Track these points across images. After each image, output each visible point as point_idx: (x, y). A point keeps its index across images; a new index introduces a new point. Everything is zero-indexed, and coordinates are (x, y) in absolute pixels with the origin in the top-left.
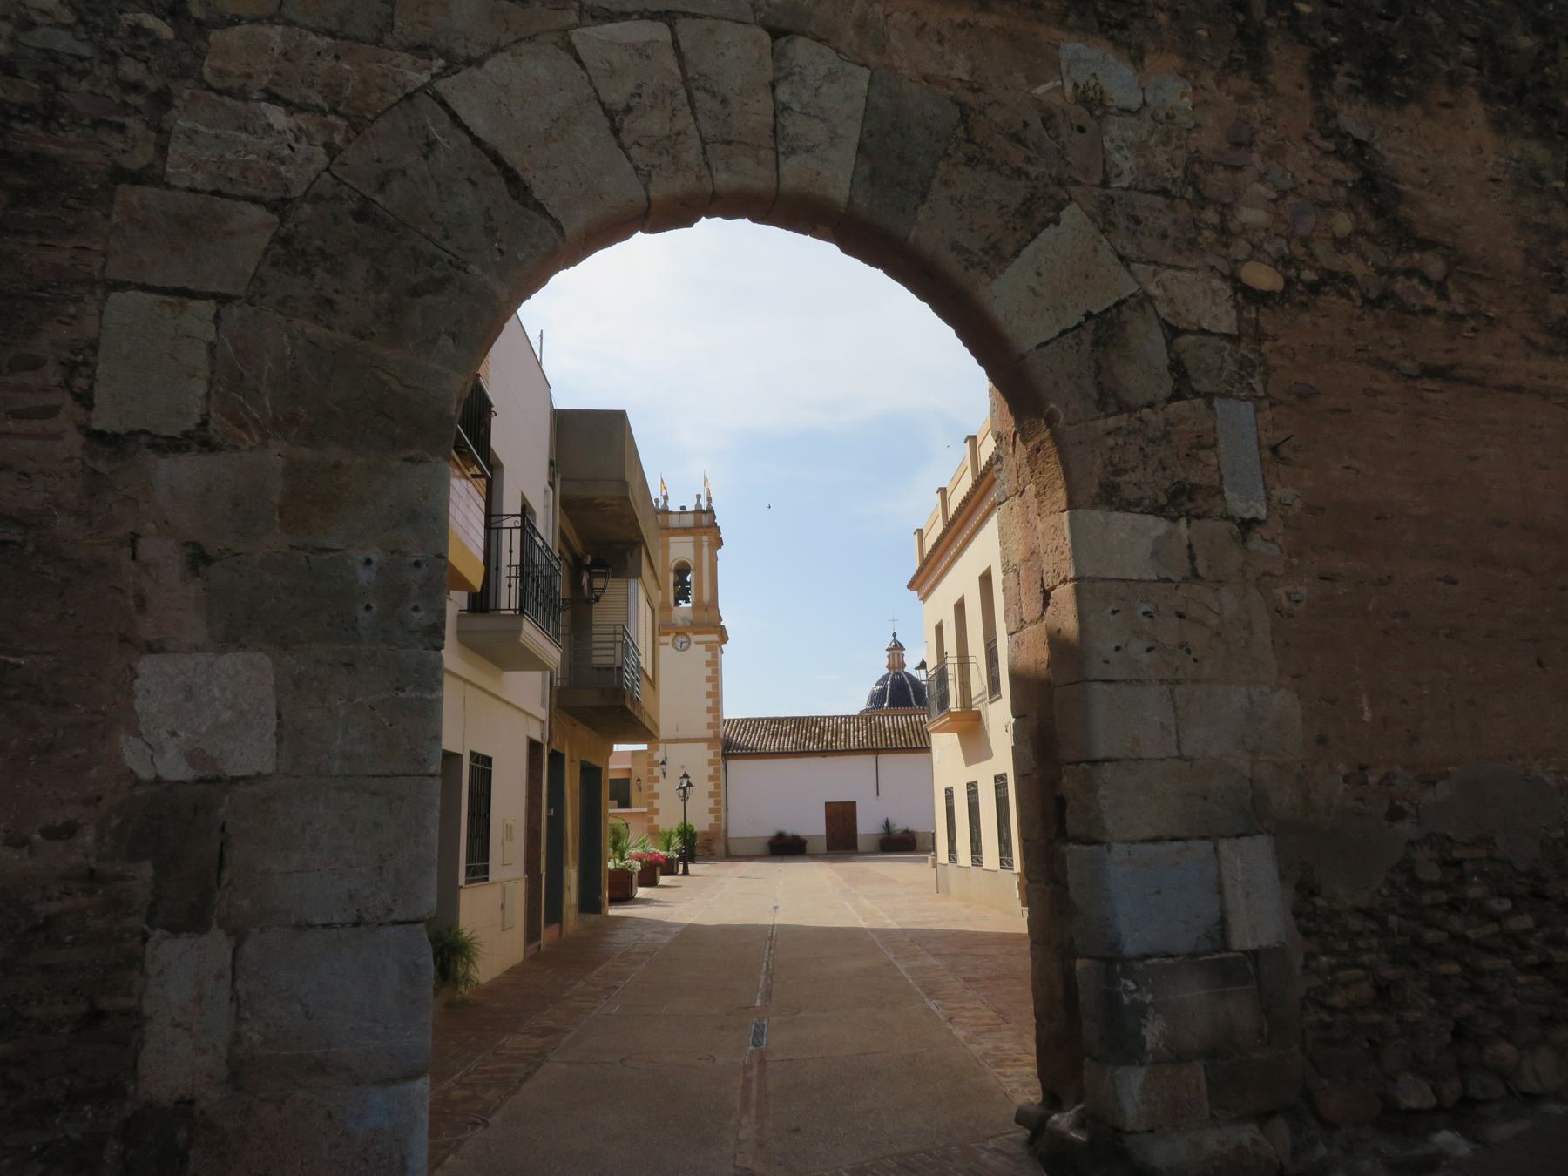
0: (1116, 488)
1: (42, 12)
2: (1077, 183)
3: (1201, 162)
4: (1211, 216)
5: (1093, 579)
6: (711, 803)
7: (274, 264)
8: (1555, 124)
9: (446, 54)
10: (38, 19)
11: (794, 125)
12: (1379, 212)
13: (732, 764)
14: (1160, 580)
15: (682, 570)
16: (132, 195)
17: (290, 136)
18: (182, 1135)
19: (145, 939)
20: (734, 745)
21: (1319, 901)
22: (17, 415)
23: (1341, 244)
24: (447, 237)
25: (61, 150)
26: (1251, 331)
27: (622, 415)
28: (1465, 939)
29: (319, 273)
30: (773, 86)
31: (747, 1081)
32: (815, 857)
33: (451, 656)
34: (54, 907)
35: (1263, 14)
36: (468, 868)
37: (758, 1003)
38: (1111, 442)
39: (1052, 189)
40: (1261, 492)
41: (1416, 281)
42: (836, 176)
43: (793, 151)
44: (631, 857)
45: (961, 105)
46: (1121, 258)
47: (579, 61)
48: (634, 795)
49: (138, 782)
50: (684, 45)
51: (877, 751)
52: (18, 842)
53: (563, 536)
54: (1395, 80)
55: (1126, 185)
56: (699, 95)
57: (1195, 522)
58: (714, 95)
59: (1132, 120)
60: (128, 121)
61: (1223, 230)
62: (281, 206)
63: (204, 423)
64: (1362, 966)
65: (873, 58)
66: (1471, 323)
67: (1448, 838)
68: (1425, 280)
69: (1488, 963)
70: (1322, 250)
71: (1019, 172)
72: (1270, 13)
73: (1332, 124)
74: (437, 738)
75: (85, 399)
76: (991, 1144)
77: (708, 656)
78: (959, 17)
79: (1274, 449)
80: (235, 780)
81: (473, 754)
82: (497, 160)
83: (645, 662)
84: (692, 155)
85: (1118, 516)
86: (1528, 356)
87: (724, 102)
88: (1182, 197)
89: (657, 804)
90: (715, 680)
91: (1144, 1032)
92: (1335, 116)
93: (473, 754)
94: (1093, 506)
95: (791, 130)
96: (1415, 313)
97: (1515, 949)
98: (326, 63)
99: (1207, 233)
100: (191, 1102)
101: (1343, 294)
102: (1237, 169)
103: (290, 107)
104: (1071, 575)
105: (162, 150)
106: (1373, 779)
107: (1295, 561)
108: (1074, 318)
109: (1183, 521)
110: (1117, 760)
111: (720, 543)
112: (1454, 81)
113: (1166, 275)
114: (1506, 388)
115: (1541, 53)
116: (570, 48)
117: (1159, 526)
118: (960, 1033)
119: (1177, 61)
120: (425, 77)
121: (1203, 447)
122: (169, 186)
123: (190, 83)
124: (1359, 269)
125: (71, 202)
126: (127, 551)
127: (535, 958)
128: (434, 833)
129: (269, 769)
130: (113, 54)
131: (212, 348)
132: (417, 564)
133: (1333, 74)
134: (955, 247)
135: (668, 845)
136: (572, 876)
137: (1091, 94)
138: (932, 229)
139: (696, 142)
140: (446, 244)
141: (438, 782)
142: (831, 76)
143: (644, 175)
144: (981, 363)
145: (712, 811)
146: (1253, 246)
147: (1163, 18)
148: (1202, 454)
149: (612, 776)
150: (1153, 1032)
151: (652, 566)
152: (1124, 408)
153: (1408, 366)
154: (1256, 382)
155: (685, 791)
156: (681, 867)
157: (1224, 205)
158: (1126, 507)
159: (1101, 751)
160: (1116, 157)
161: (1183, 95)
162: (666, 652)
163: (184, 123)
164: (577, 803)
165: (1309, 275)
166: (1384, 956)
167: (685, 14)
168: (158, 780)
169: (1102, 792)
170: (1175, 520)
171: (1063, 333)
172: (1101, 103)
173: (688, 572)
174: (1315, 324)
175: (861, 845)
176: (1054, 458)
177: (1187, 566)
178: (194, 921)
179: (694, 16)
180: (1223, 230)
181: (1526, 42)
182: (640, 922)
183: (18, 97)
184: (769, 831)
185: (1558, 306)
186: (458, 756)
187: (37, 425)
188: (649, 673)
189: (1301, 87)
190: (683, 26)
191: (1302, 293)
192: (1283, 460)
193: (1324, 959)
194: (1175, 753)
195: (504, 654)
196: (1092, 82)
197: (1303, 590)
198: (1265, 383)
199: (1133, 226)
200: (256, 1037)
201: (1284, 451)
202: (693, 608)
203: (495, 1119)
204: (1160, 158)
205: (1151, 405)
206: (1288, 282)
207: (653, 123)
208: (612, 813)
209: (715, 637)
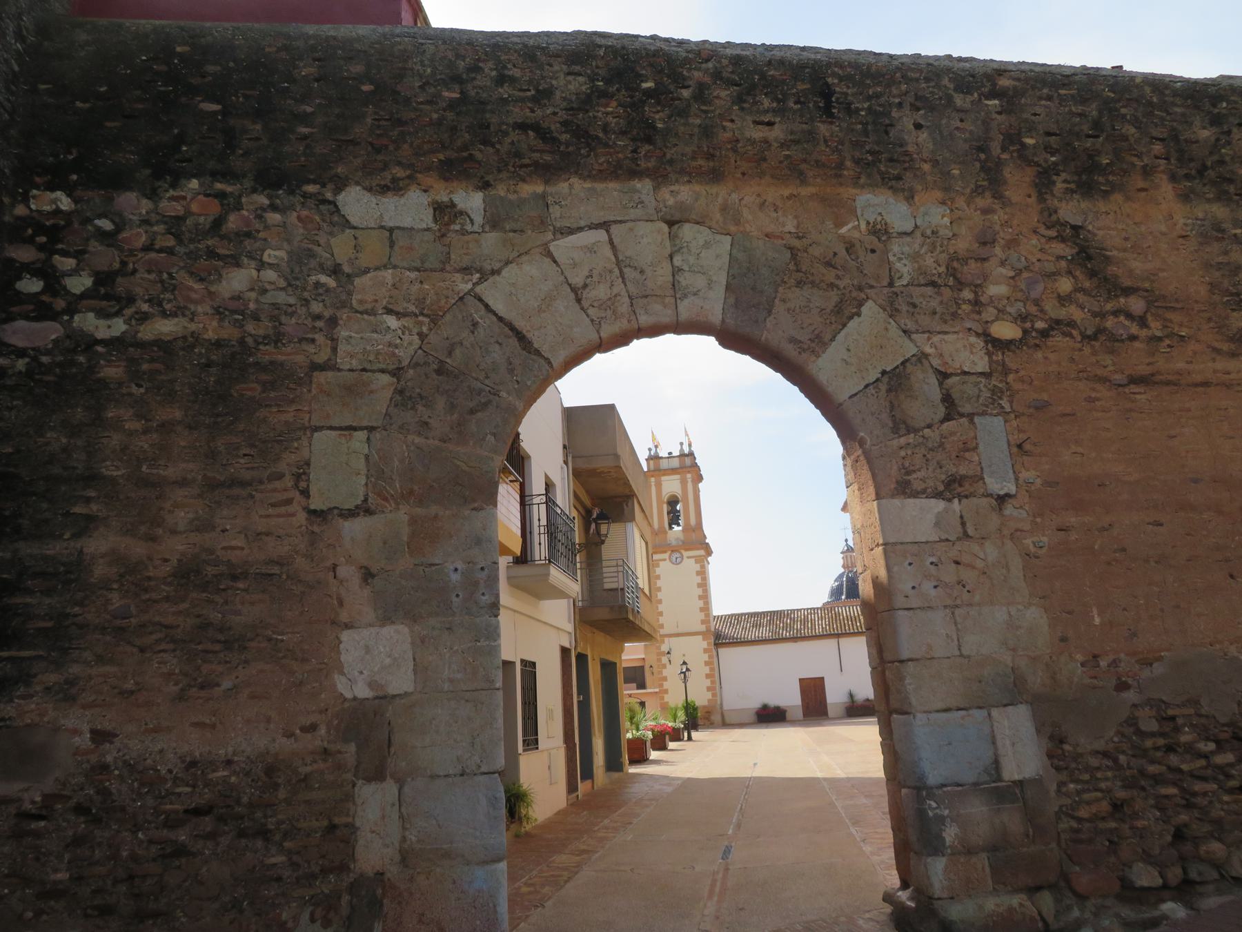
0: (908, 483)
1: (270, 283)
2: (872, 287)
3: (958, 260)
4: (967, 294)
5: (895, 544)
6: (708, 683)
7: (396, 406)
8: (1232, 189)
9: (480, 271)
10: (268, 287)
11: (685, 280)
12: (1092, 274)
13: (722, 651)
14: (941, 541)
15: (673, 502)
16: (321, 377)
17: (400, 332)
18: (379, 891)
19: (354, 786)
20: (723, 637)
21: (1067, 747)
22: (273, 505)
23: (1063, 300)
24: (487, 377)
25: (284, 358)
26: (1000, 368)
27: (611, 408)
28: (1180, 771)
29: (420, 408)
30: (671, 257)
31: (714, 881)
32: (794, 723)
33: (506, 597)
34: (309, 769)
35: (999, 151)
36: (524, 741)
37: (730, 832)
38: (903, 453)
39: (854, 294)
40: (1011, 475)
41: (1122, 318)
42: (715, 305)
43: (685, 296)
44: (646, 729)
45: (791, 249)
46: (905, 332)
47: (555, 262)
48: (649, 679)
49: (345, 699)
50: (616, 241)
51: (838, 636)
52: (289, 735)
53: (576, 496)
54: (1101, 179)
55: (905, 283)
56: (626, 270)
57: (964, 501)
58: (635, 268)
59: (908, 239)
60: (316, 336)
61: (976, 303)
62: (396, 373)
63: (366, 500)
64: (1101, 790)
65: (733, 229)
66: (1167, 342)
67: (1163, 702)
68: (1129, 316)
69: (1198, 787)
70: (1048, 307)
71: (832, 286)
72: (1004, 149)
73: (1054, 218)
74: (495, 650)
75: (306, 493)
76: (867, 915)
77: (698, 567)
78: (787, 192)
79: (1020, 446)
80: (394, 696)
81: (522, 661)
82: (512, 328)
83: (643, 582)
84: (624, 308)
85: (911, 501)
86: (1214, 360)
87: (642, 272)
88: (946, 285)
89: (666, 685)
90: (704, 585)
91: (944, 835)
92: (1056, 212)
93: (522, 661)
94: (893, 496)
95: (684, 283)
96: (1122, 341)
97: (1221, 777)
98: (417, 286)
99: (964, 307)
100: (382, 874)
101: (1065, 334)
102: (985, 260)
103: (399, 315)
104: (881, 541)
105: (334, 350)
106: (1103, 664)
107: (1039, 520)
108: (874, 375)
109: (956, 501)
110: (917, 660)
111: (700, 478)
112: (1147, 172)
113: (936, 339)
114: (1196, 385)
115: (1218, 140)
116: (549, 255)
117: (940, 505)
118: (867, 849)
119: (939, 194)
120: (470, 286)
121: (968, 450)
122: (339, 370)
123: (346, 310)
124: (1077, 314)
125: (291, 386)
126: (331, 574)
127: (576, 805)
128: (500, 722)
129: (411, 689)
130: (306, 300)
131: (367, 457)
132: (482, 569)
133: (1054, 183)
134: (793, 340)
135: (675, 718)
136: (598, 744)
137: (879, 227)
138: (775, 332)
139: (627, 300)
140: (487, 382)
141: (500, 693)
142: (707, 245)
143: (596, 324)
144: (817, 407)
145: (709, 689)
146: (999, 311)
147: (926, 167)
148: (967, 455)
149: (624, 665)
150: (950, 834)
151: (643, 511)
152: (910, 430)
153: (1118, 378)
154: (1005, 403)
155: (684, 675)
156: (686, 734)
157: (976, 286)
158: (915, 495)
159: (905, 655)
160: (898, 265)
161: (943, 216)
162: (665, 568)
163: (344, 333)
164: (598, 686)
165: (1040, 325)
166: (1119, 783)
167: (615, 222)
168: (355, 699)
169: (907, 681)
170: (950, 500)
171: (867, 386)
172: (886, 232)
173: (677, 502)
174: (1046, 358)
175: (831, 713)
176: (866, 467)
177: (960, 529)
178: (378, 775)
179: (621, 222)
180: (976, 303)
181: (1205, 134)
182: (651, 776)
183: (261, 332)
184: (756, 704)
185: (1241, 320)
186: (513, 663)
187: (282, 510)
188: (647, 591)
189: (1030, 196)
190: (615, 229)
191: (1035, 338)
192: (1026, 453)
193: (1072, 786)
194: (957, 653)
195: (541, 590)
196: (879, 219)
197: (1045, 539)
198: (1011, 402)
199: (911, 310)
200: (413, 838)
201: (1027, 447)
202: (683, 531)
203: (549, 904)
204: (929, 261)
205: (929, 426)
206: (1025, 332)
207: (600, 292)
208: (628, 694)
209: (702, 552)
